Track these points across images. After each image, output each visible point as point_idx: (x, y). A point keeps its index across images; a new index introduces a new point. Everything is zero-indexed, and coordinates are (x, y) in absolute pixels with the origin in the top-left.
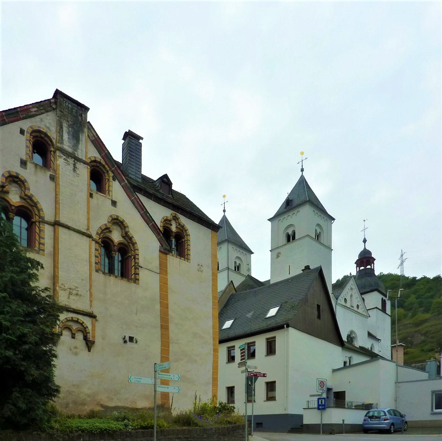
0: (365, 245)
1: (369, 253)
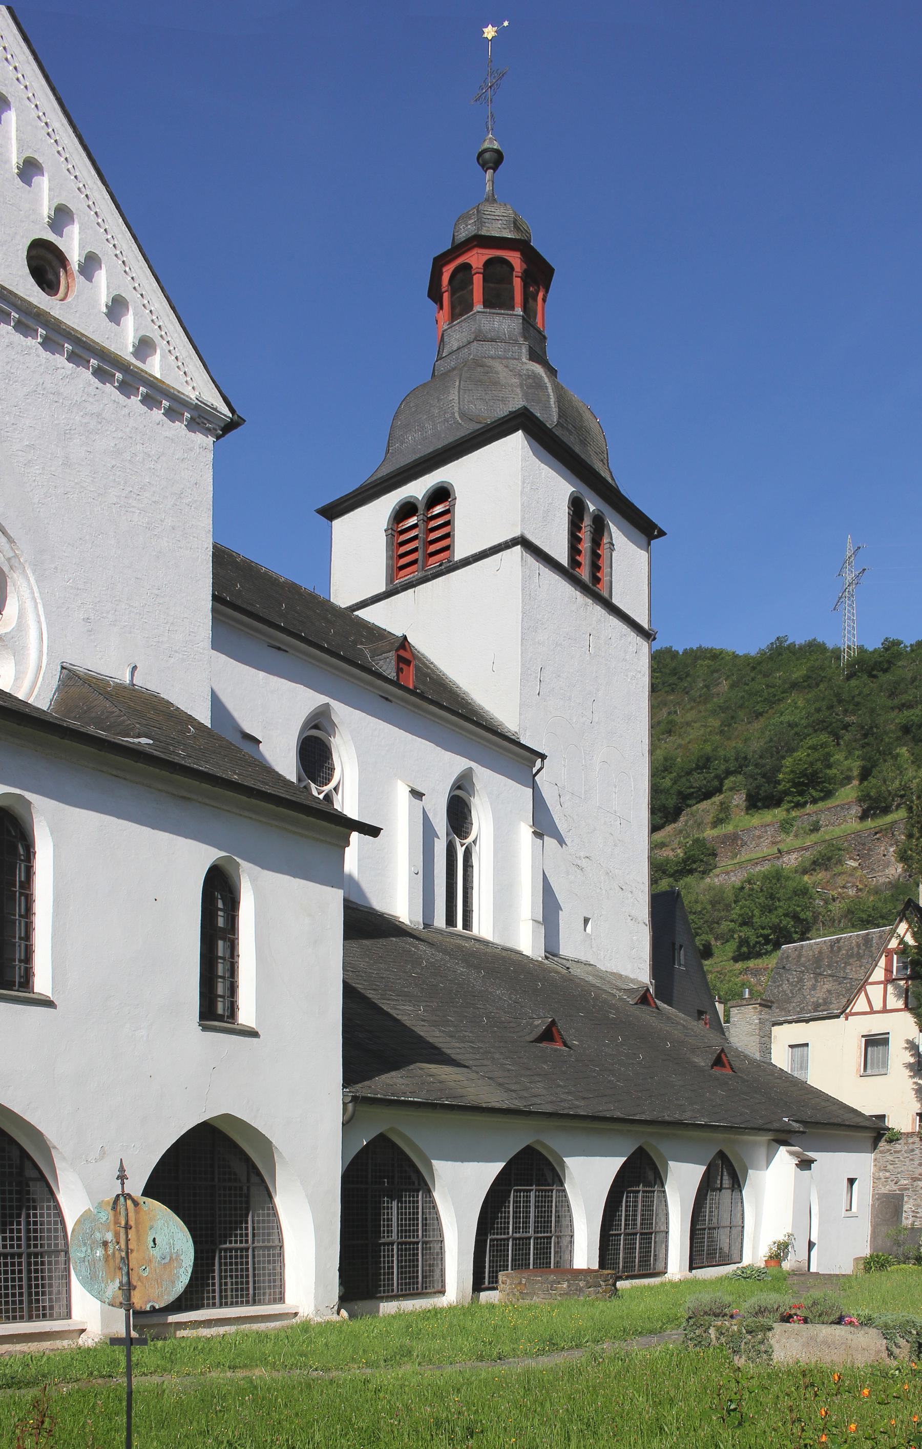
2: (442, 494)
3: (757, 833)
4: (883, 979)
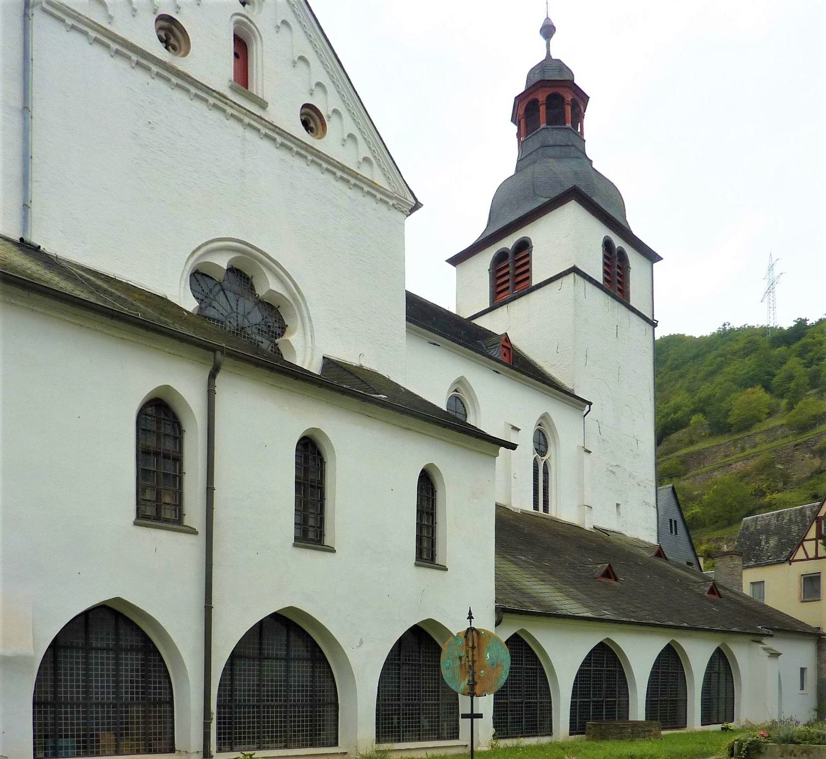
0: (548, 46)
2: (524, 246)
3: (714, 450)
4: (815, 537)
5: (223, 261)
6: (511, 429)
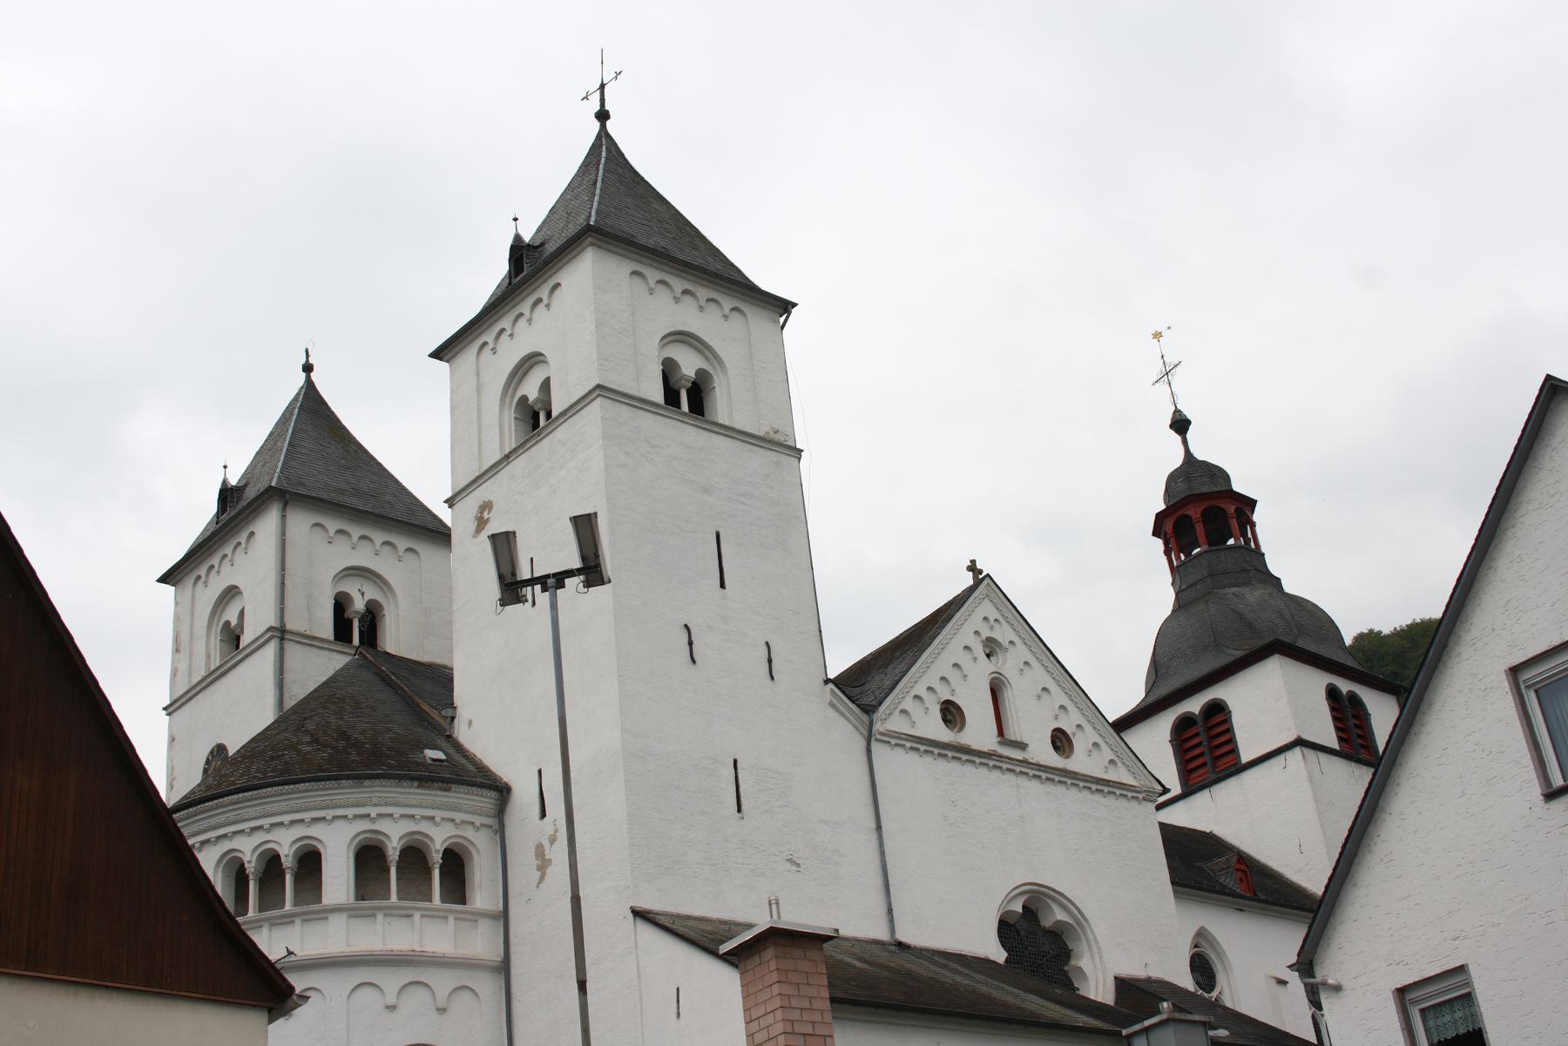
0: (1185, 442)
1: (1217, 474)
2: (1217, 710)
5: (1018, 907)
6: (1276, 985)
